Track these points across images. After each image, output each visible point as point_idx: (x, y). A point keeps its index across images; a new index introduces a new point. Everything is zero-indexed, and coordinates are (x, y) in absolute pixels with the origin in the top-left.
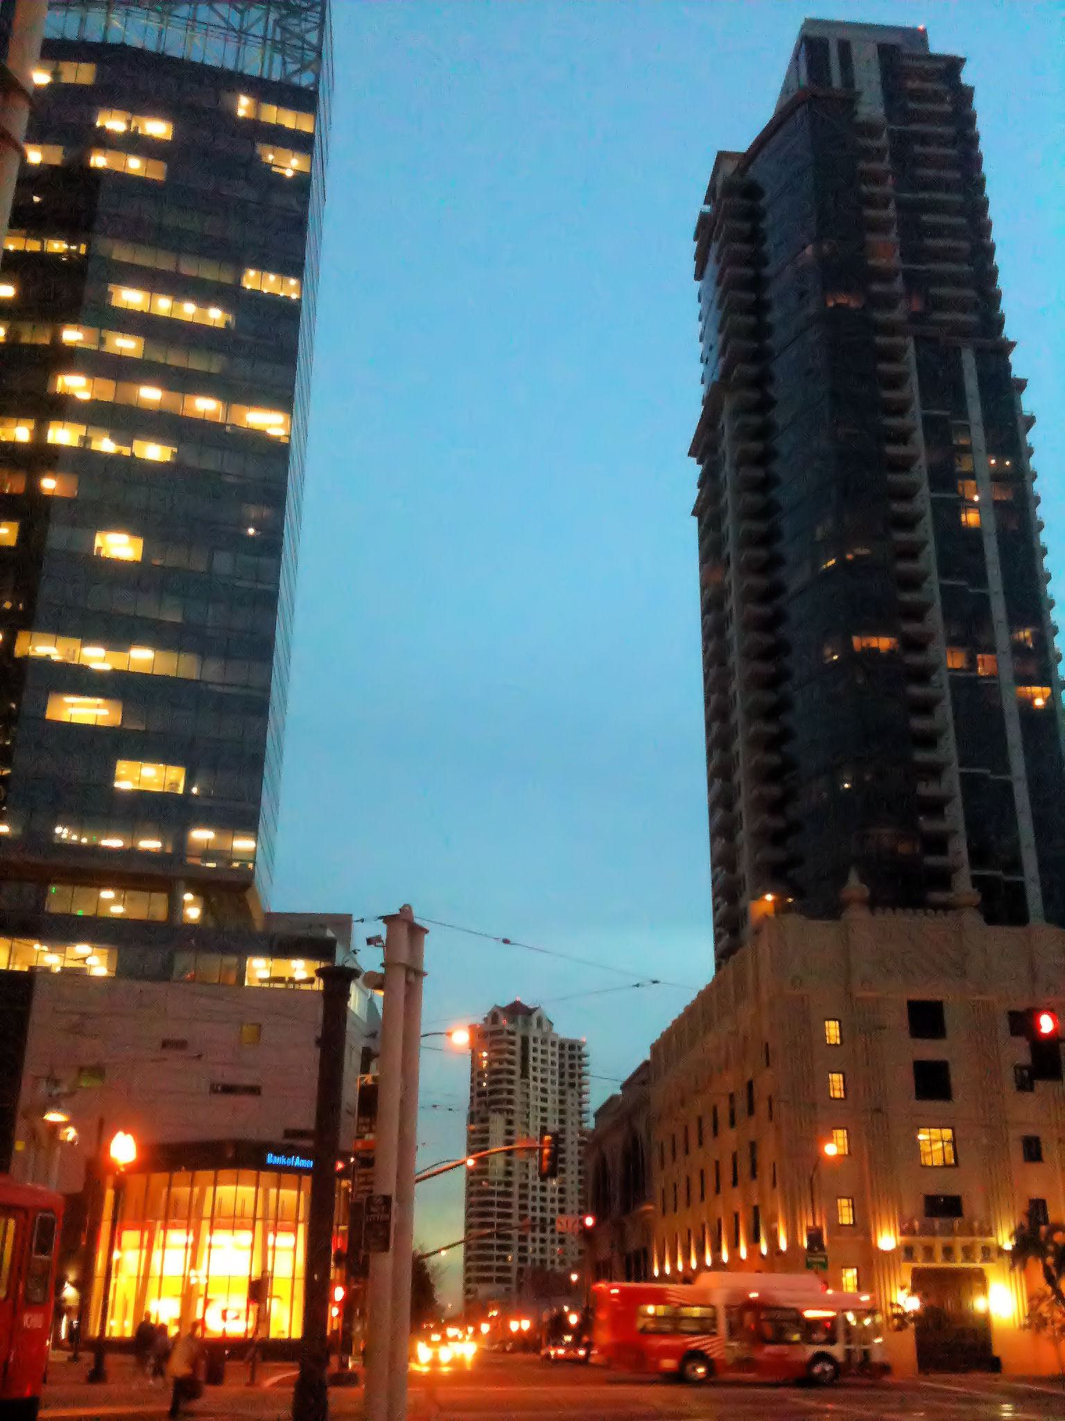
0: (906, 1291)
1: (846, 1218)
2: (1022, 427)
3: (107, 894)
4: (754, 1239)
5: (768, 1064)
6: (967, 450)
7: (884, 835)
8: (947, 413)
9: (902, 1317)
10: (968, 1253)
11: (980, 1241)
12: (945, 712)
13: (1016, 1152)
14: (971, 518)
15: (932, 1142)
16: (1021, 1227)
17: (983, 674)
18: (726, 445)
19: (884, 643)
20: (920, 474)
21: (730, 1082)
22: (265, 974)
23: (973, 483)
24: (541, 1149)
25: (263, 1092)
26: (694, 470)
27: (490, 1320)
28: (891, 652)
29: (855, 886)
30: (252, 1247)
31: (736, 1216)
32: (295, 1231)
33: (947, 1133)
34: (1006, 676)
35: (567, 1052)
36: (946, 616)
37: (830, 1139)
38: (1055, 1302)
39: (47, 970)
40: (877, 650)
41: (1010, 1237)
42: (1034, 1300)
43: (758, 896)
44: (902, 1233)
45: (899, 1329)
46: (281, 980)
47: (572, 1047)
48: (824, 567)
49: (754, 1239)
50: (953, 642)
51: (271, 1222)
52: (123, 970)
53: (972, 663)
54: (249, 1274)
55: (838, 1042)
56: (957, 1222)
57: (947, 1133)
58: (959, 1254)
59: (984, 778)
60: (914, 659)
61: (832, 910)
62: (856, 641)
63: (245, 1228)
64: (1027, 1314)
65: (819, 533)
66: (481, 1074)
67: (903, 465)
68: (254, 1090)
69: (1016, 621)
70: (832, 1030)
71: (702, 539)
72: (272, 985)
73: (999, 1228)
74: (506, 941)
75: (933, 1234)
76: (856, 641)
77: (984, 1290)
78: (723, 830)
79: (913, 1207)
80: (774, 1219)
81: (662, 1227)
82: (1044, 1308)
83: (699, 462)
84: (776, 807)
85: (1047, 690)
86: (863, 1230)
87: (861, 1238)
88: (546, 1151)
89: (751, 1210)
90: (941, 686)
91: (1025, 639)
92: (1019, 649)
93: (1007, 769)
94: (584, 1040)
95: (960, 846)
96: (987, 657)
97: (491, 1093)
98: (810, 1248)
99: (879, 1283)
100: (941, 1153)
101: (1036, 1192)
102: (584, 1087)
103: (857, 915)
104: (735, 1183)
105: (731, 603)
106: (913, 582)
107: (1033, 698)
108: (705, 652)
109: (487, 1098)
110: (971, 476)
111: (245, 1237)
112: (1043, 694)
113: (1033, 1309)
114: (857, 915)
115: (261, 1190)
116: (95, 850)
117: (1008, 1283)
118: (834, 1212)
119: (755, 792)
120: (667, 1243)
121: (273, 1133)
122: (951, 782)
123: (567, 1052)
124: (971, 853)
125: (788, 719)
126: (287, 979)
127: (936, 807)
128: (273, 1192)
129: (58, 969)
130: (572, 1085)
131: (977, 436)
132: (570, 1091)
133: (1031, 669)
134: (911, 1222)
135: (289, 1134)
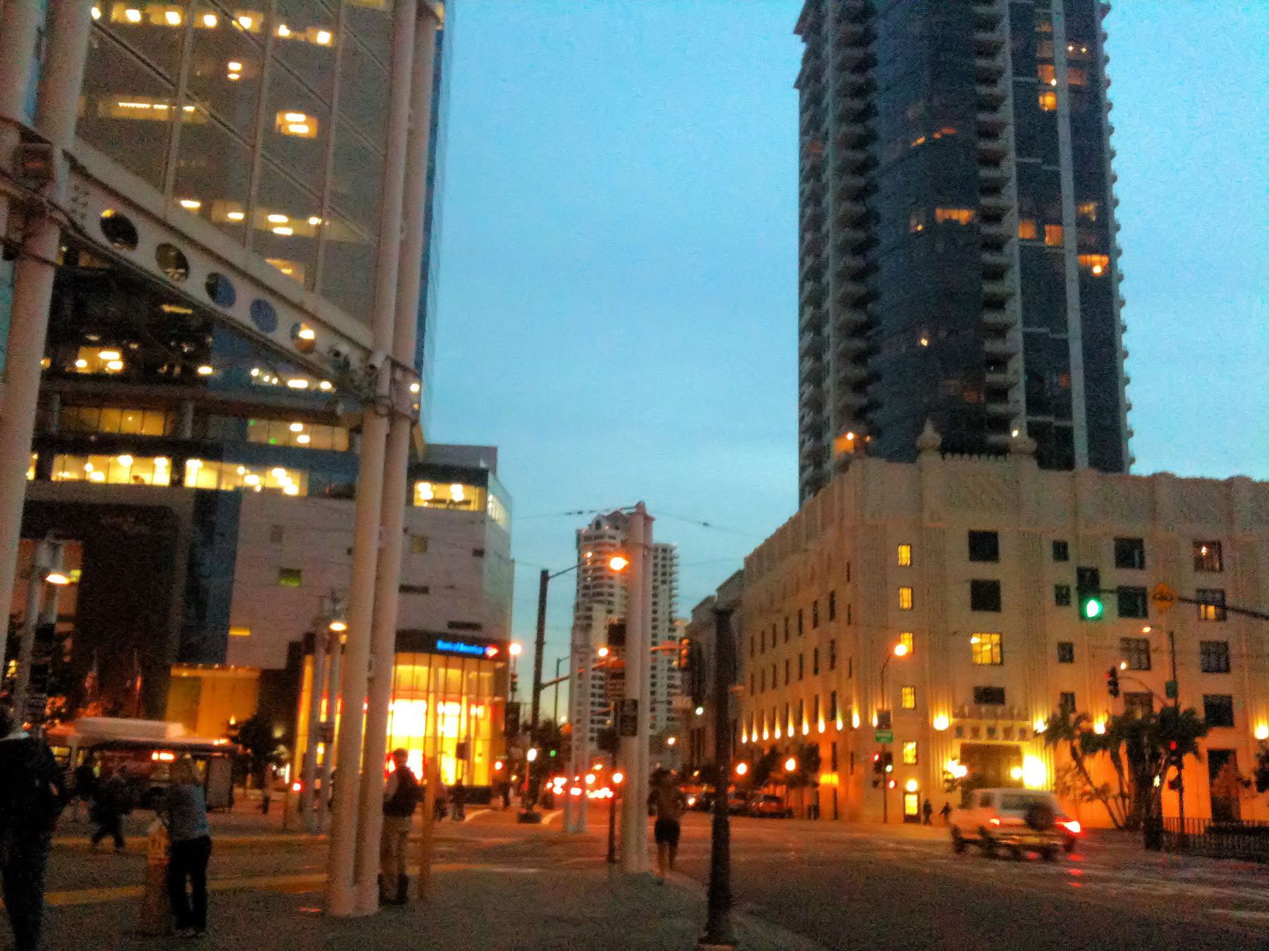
0: (957, 761)
1: (909, 702)
2: (1097, 14)
3: (296, 427)
4: (831, 717)
5: (849, 580)
6: (1049, 36)
7: (952, 385)
8: (1040, 161)
9: (952, 781)
10: (1008, 733)
11: (1019, 724)
12: (1013, 281)
13: (1053, 651)
14: (1048, 101)
15: (982, 645)
16: (1054, 716)
17: (1049, 244)
18: (828, 26)
19: (963, 215)
20: (1004, 60)
21: (814, 592)
22: (430, 496)
23: (1051, 68)
24: (680, 651)
25: (431, 592)
26: (798, 48)
27: (595, 772)
28: (970, 224)
29: (930, 435)
30: (460, 716)
31: (817, 698)
32: (460, 702)
33: (996, 638)
34: (1071, 244)
35: (660, 555)
36: (1022, 193)
37: (899, 641)
38: (1078, 773)
39: (249, 490)
40: (957, 222)
41: (1045, 723)
42: (1060, 772)
43: (840, 434)
44: (955, 716)
45: (949, 791)
46: (443, 501)
47: (664, 550)
48: (914, 144)
49: (831, 717)
50: (1023, 214)
51: (441, 695)
52: (314, 491)
53: (1041, 234)
54: (423, 735)
55: (909, 563)
56: (1000, 709)
57: (996, 638)
58: (1000, 734)
59: (1049, 425)
60: (989, 230)
61: (908, 453)
62: (939, 212)
63: (421, 699)
64: (1053, 782)
65: (910, 114)
66: (585, 571)
67: (990, 51)
68: (425, 590)
69: (1081, 198)
70: (904, 554)
71: (803, 111)
72: (436, 506)
73: (1034, 708)
74: (705, 524)
75: (980, 717)
76: (939, 212)
77: (1020, 762)
78: (812, 378)
79: (965, 696)
80: (848, 702)
81: (749, 705)
82: (1068, 778)
83: (804, 40)
84: (860, 358)
85: (1105, 259)
86: (922, 713)
87: (920, 719)
88: (684, 652)
89: (829, 696)
90: (1011, 255)
91: (1089, 213)
92: (1082, 221)
93: (1064, 325)
94: (675, 544)
95: (1018, 396)
96: (1054, 228)
97: (594, 587)
98: (880, 727)
99: (934, 758)
100: (989, 654)
101: (1067, 688)
102: (674, 584)
103: (930, 460)
104: (816, 671)
105: (828, 175)
106: (993, 160)
107: (1092, 265)
108: (802, 216)
109: (592, 591)
110: (1049, 61)
111: (420, 705)
112: (1101, 263)
113: (1058, 778)
114: (930, 460)
115: (432, 669)
116: (283, 390)
117: (1044, 759)
118: (899, 699)
119: (842, 346)
120: (754, 716)
121: (440, 626)
122: (1015, 340)
123: (660, 555)
124: (1028, 401)
125: (873, 280)
126: (448, 502)
127: (1000, 362)
128: (442, 671)
129: (258, 489)
130: (664, 582)
131: (1059, 25)
132: (662, 587)
133: (1092, 241)
134: (962, 708)
135: (452, 625)
